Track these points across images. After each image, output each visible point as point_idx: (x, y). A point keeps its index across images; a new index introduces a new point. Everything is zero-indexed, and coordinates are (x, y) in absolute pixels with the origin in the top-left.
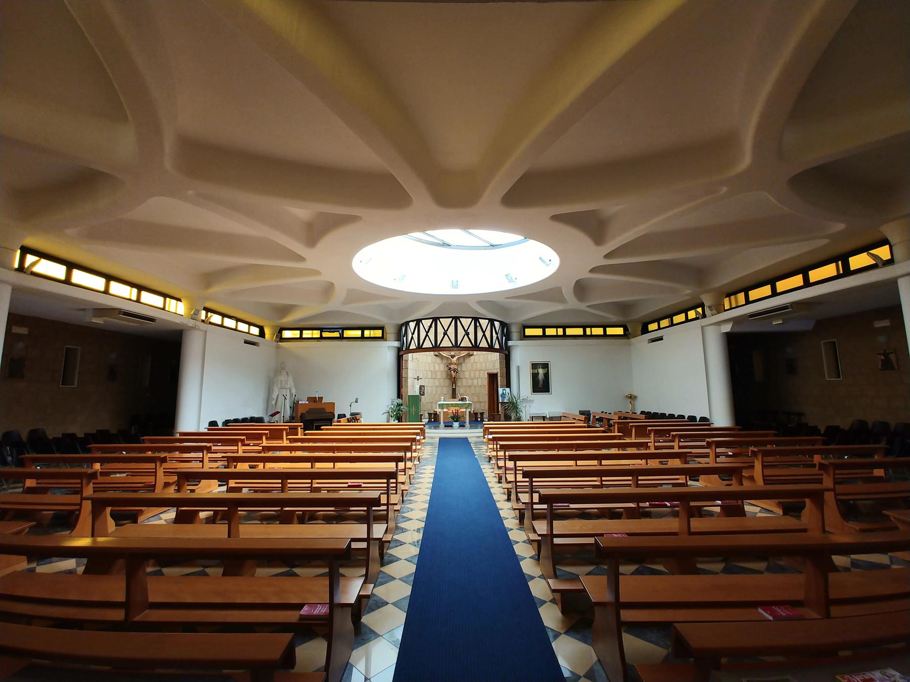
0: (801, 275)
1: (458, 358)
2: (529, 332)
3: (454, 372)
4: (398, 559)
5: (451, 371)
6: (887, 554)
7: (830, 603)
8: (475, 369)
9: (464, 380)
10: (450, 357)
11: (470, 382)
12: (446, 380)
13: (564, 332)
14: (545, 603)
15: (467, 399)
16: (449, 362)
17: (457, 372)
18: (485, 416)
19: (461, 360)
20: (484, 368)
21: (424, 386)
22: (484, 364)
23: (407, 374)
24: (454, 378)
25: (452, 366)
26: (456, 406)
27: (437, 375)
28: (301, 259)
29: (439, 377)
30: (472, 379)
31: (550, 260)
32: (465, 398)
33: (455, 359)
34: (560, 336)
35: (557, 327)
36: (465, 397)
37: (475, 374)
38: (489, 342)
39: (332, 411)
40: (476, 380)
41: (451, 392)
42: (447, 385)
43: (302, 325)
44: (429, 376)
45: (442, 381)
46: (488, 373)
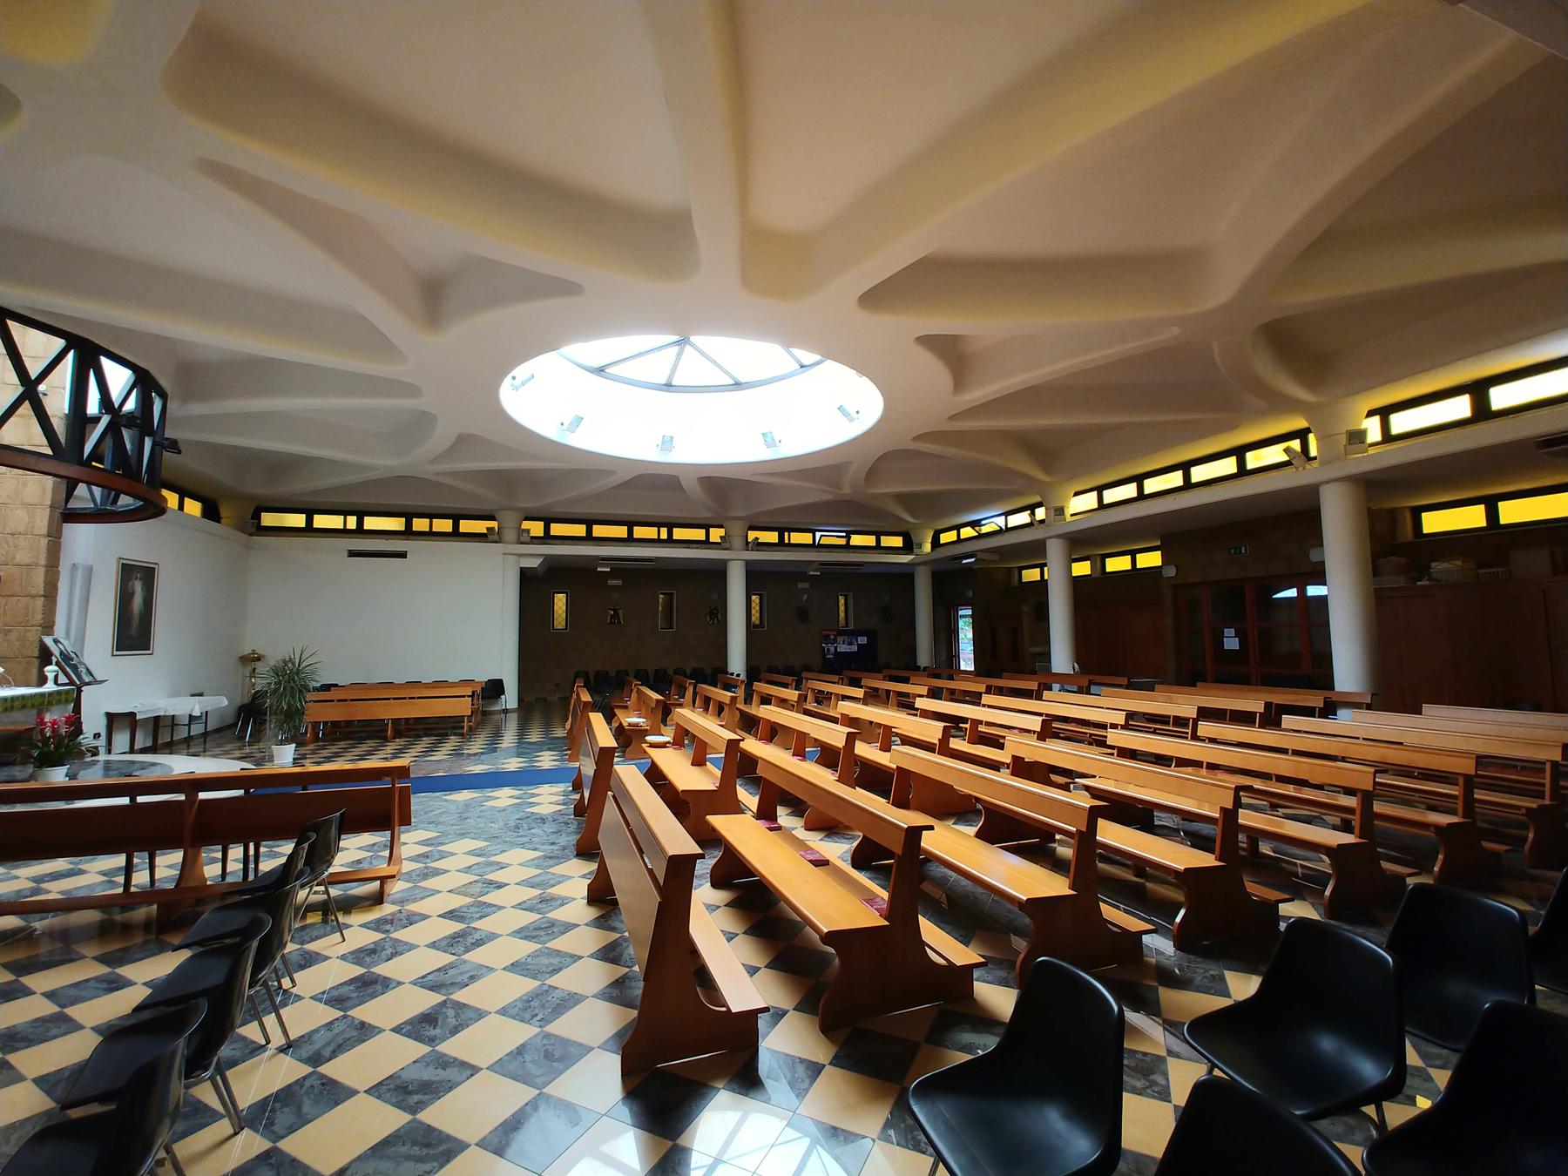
0: (1181, 471)
2: (268, 519)
4: (480, 1014)
6: (286, 943)
13: (670, 534)
14: (591, 1051)
28: (383, 346)
31: (858, 412)
34: (351, 531)
35: (659, 525)
39: (152, 720)
43: (783, 521)
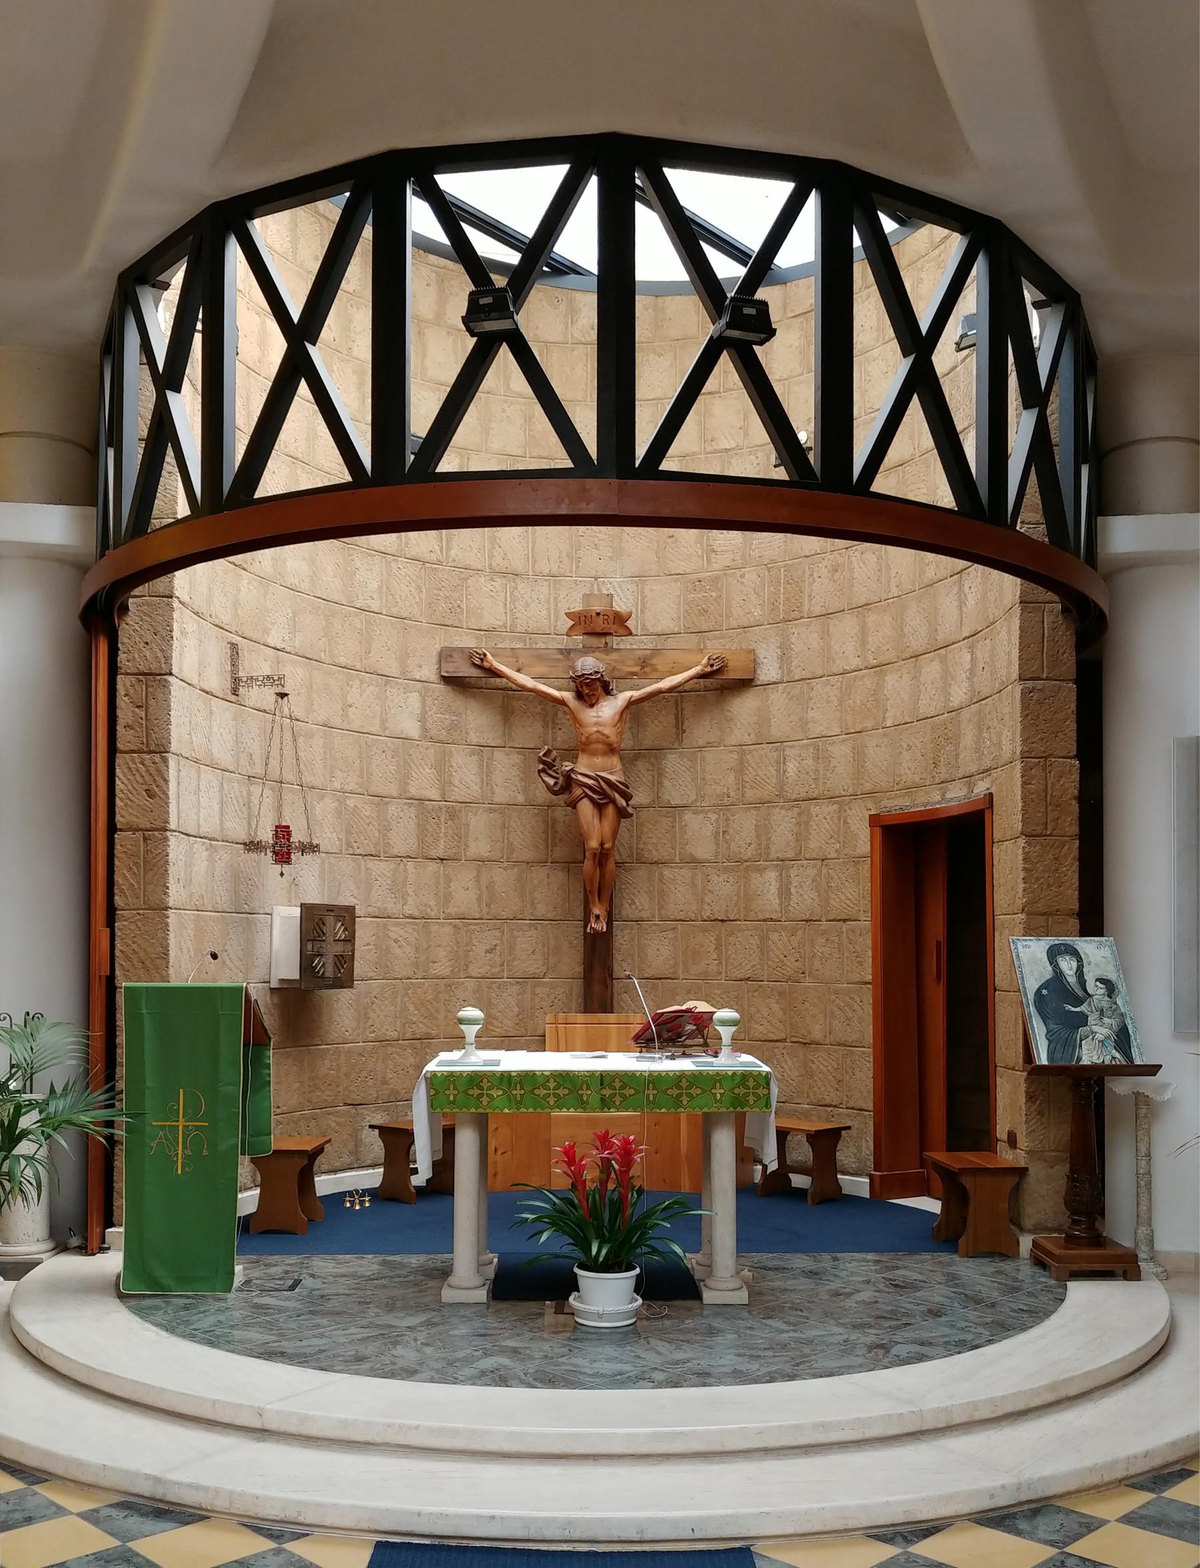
1: (631, 704)
3: (599, 807)
5: (573, 805)
7: (453, 815)
8: (767, 792)
9: (678, 879)
10: (568, 696)
11: (722, 886)
12: (540, 873)
15: (726, 1033)
16: (562, 737)
17: (622, 814)
18: (845, 1154)
19: (657, 727)
20: (840, 778)
21: (347, 915)
22: (841, 752)
23: (156, 792)
24: (602, 857)
25: (585, 767)
26: (605, 1104)
27: (460, 837)
29: (480, 846)
30: (742, 866)
32: (703, 1022)
33: (608, 710)
36: (702, 1007)
37: (762, 831)
38: (971, 447)
40: (772, 875)
41: (571, 962)
42: (542, 910)
44: (403, 837)
45: (502, 878)
46: (874, 820)
